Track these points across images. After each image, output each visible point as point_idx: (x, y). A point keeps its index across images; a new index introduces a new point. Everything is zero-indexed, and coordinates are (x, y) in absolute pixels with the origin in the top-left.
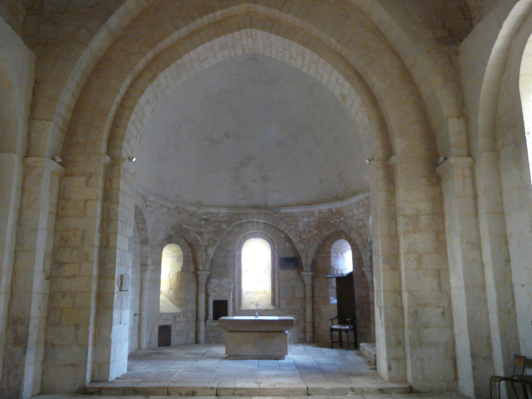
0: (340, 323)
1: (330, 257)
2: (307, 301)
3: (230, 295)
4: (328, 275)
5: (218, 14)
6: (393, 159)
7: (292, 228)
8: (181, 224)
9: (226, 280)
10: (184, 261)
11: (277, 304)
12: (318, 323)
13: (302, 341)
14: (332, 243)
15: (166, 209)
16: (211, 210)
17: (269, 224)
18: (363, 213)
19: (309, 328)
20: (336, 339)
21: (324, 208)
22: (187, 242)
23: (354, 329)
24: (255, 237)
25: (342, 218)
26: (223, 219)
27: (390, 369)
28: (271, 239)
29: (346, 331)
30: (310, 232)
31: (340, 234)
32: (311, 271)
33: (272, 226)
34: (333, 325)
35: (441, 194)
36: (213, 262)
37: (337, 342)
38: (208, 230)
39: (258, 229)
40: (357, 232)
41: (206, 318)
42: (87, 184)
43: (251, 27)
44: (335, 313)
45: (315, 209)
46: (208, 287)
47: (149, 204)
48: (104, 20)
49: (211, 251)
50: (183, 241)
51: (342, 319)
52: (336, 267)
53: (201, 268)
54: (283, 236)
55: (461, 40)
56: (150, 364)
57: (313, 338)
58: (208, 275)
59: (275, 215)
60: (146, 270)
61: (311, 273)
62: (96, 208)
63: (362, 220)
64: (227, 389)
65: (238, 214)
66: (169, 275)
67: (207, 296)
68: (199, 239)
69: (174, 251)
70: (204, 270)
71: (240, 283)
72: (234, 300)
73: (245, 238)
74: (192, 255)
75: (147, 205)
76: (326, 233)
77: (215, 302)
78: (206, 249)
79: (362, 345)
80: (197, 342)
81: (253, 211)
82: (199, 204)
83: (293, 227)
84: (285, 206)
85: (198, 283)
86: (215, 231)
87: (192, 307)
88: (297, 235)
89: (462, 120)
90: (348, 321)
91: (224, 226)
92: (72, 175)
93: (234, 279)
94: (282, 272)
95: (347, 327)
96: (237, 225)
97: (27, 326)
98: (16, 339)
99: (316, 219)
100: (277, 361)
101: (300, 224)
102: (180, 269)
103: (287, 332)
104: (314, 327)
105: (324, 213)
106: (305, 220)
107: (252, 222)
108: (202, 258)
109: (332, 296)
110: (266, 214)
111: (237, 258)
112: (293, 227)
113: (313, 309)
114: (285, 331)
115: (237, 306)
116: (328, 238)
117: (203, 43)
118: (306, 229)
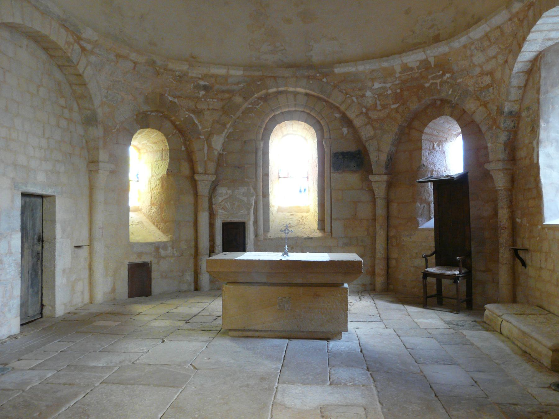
0: (438, 264)
1: (421, 149)
2: (377, 225)
3: (249, 214)
4: (420, 178)
7: (353, 102)
8: (162, 95)
9: (243, 190)
10: (171, 159)
11: (328, 228)
12: (397, 260)
15: (131, 65)
17: (313, 96)
18: (495, 57)
19: (380, 268)
20: (432, 290)
21: (413, 59)
22: (176, 127)
23: (468, 276)
24: (292, 119)
25: (448, 75)
26: (235, 87)
28: (318, 122)
29: (455, 278)
30: (384, 107)
31: (440, 107)
32: (386, 174)
33: (319, 98)
34: (427, 267)
37: (430, 297)
38: (211, 107)
39: (295, 105)
40: (478, 99)
45: (396, 63)
46: (213, 200)
47: (89, 47)
49: (218, 142)
50: (168, 124)
51: (443, 256)
52: (431, 167)
53: (200, 169)
54: (338, 115)
56: (154, 305)
57: (389, 288)
58: (213, 182)
59: (325, 80)
60: (97, 171)
61: (385, 178)
63: (491, 73)
65: (261, 79)
66: (150, 181)
67: (212, 215)
68: (197, 122)
69: (155, 143)
70: (205, 174)
71: (266, 195)
72: (256, 222)
74: (186, 147)
75: (83, 49)
76: (414, 106)
77: (227, 226)
78: (208, 139)
80: (197, 289)
81: (287, 73)
82: (193, 60)
83: (354, 99)
84: (341, 62)
85: (196, 194)
86: (223, 108)
87: (188, 233)
90: (459, 261)
91: (238, 99)
93: (255, 188)
94: (335, 175)
96: (260, 98)
99: (397, 82)
100: (325, 342)
101: (368, 93)
102: (165, 172)
103: (346, 285)
104: (388, 267)
105: (412, 69)
106: (377, 85)
107: (286, 92)
108: (201, 153)
109: (421, 216)
110: (308, 77)
111: (260, 153)
112: (354, 99)
114: (343, 284)
115: (261, 231)
116: (416, 116)
118: (378, 102)
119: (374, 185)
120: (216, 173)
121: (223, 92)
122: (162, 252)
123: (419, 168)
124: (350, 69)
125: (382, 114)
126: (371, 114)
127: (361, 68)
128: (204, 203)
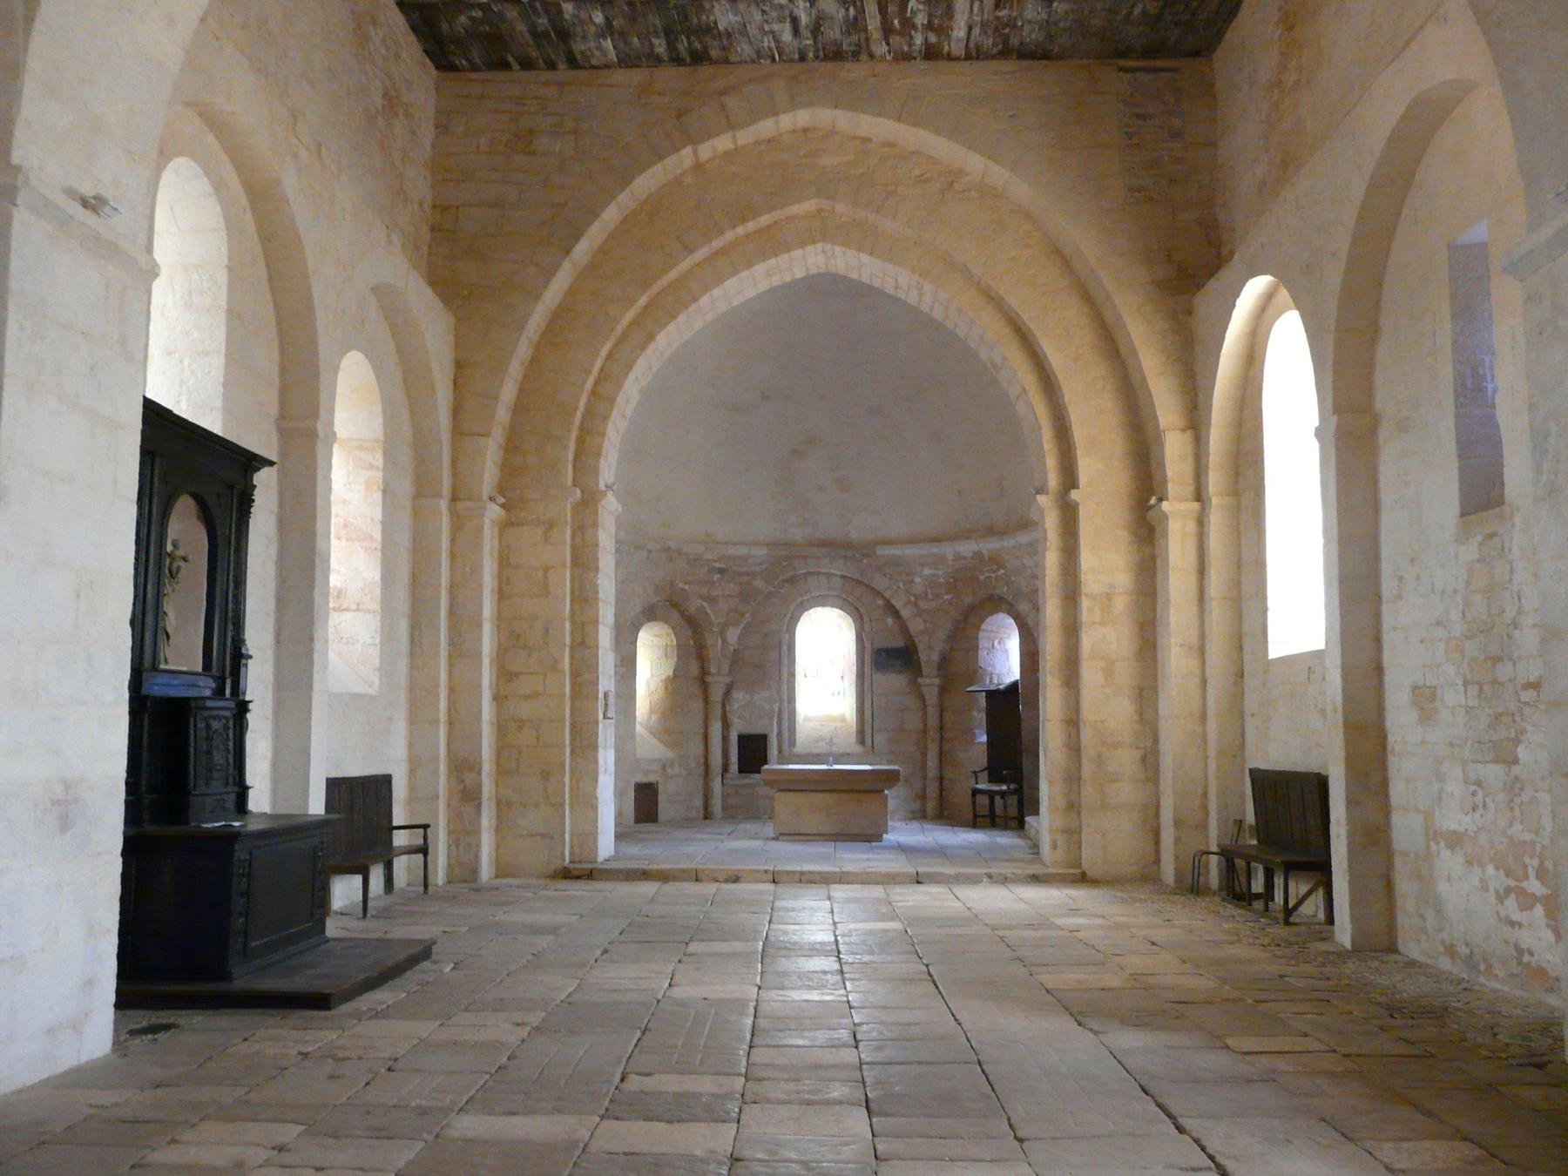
5: (765, 220)
6: (1074, 495)
9: (765, 694)
13: (920, 815)
14: (982, 620)
15: (645, 554)
16: (733, 551)
19: (932, 789)
21: (967, 548)
23: (1019, 791)
26: (757, 569)
27: (1055, 847)
29: (1003, 794)
31: (994, 603)
33: (858, 582)
35: (1153, 558)
36: (736, 660)
37: (987, 819)
41: (725, 769)
42: (546, 538)
43: (824, 240)
44: (984, 761)
45: (948, 550)
48: (567, 251)
49: (733, 635)
50: (675, 615)
53: (713, 670)
55: (1199, 286)
57: (941, 809)
61: (937, 681)
62: (564, 582)
64: (788, 873)
71: (792, 700)
72: (779, 734)
73: (803, 607)
76: (968, 599)
77: (744, 740)
78: (722, 634)
79: (1028, 819)
80: (707, 816)
87: (696, 748)
88: (909, 602)
89: (1189, 434)
92: (519, 524)
93: (779, 691)
94: (878, 677)
95: (1004, 787)
97: (479, 774)
98: (464, 791)
101: (917, 580)
106: (927, 571)
107: (818, 574)
111: (785, 648)
113: (941, 754)
115: (785, 746)
116: (972, 609)
117: (735, 272)
119: (924, 689)
120: (730, 673)
121: (741, 574)
122: (669, 771)
123: (976, 671)
124: (896, 551)
125: (934, 605)
126: (921, 604)
127: (908, 552)
128: (717, 711)
